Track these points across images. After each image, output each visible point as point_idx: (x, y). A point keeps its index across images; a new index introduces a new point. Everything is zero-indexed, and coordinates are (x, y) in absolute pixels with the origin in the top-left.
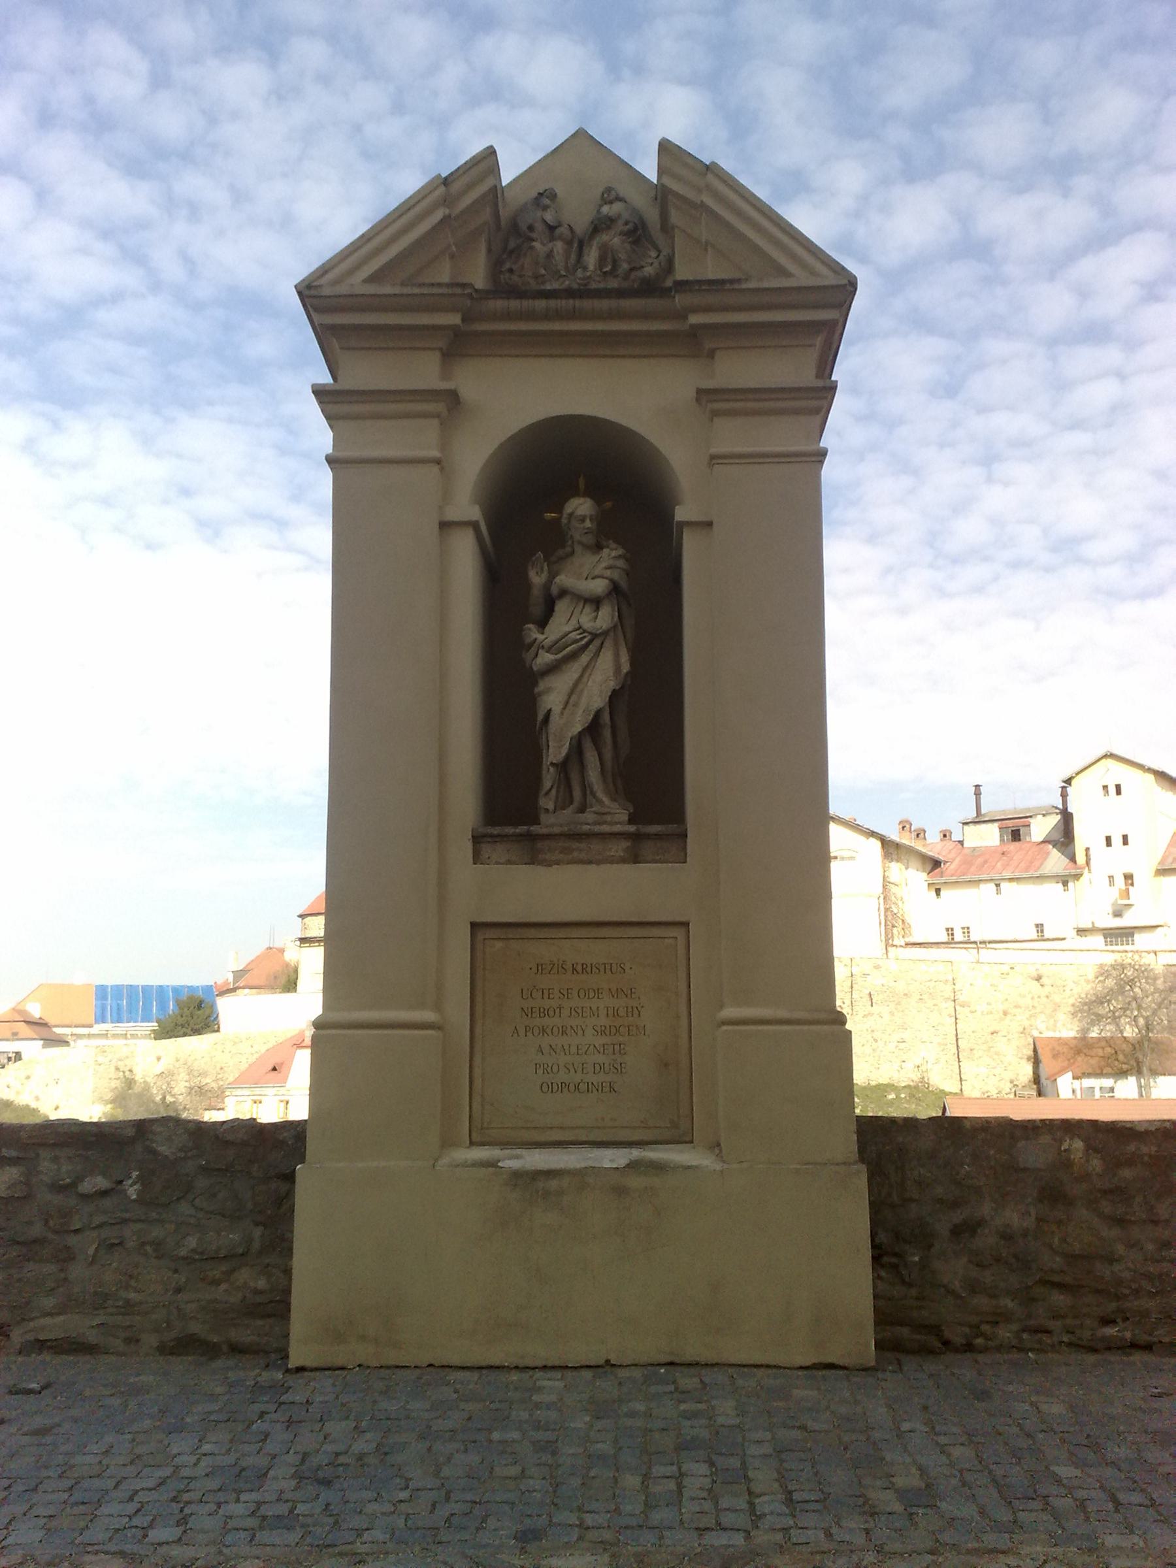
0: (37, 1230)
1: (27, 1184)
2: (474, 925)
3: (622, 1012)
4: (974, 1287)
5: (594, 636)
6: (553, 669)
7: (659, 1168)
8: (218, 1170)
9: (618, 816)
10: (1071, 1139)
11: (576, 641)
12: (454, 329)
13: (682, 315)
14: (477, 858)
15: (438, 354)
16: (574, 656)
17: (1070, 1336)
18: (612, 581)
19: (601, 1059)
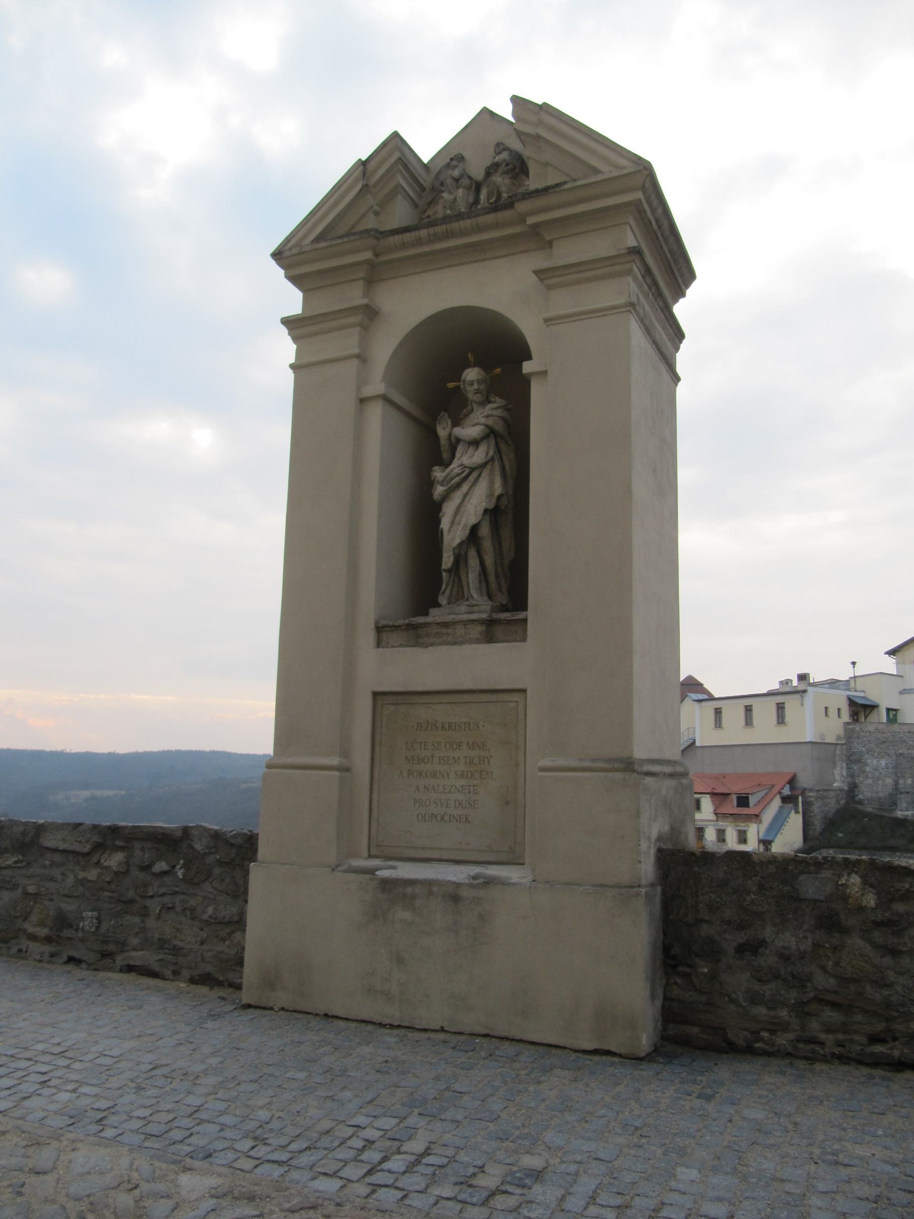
0: (131, 894)
1: (127, 863)
2: (375, 694)
3: (476, 761)
4: (755, 999)
5: (472, 470)
6: (445, 497)
7: (490, 882)
8: (226, 863)
9: (483, 608)
10: (849, 874)
11: (458, 475)
12: (369, 262)
13: (522, 219)
14: (379, 644)
15: (362, 282)
16: (458, 486)
17: (840, 1049)
18: (487, 426)
19: (460, 797)
